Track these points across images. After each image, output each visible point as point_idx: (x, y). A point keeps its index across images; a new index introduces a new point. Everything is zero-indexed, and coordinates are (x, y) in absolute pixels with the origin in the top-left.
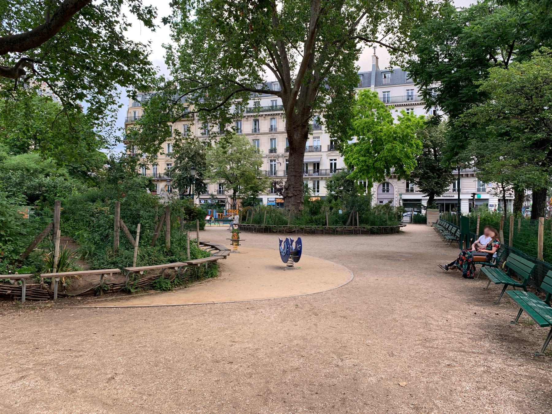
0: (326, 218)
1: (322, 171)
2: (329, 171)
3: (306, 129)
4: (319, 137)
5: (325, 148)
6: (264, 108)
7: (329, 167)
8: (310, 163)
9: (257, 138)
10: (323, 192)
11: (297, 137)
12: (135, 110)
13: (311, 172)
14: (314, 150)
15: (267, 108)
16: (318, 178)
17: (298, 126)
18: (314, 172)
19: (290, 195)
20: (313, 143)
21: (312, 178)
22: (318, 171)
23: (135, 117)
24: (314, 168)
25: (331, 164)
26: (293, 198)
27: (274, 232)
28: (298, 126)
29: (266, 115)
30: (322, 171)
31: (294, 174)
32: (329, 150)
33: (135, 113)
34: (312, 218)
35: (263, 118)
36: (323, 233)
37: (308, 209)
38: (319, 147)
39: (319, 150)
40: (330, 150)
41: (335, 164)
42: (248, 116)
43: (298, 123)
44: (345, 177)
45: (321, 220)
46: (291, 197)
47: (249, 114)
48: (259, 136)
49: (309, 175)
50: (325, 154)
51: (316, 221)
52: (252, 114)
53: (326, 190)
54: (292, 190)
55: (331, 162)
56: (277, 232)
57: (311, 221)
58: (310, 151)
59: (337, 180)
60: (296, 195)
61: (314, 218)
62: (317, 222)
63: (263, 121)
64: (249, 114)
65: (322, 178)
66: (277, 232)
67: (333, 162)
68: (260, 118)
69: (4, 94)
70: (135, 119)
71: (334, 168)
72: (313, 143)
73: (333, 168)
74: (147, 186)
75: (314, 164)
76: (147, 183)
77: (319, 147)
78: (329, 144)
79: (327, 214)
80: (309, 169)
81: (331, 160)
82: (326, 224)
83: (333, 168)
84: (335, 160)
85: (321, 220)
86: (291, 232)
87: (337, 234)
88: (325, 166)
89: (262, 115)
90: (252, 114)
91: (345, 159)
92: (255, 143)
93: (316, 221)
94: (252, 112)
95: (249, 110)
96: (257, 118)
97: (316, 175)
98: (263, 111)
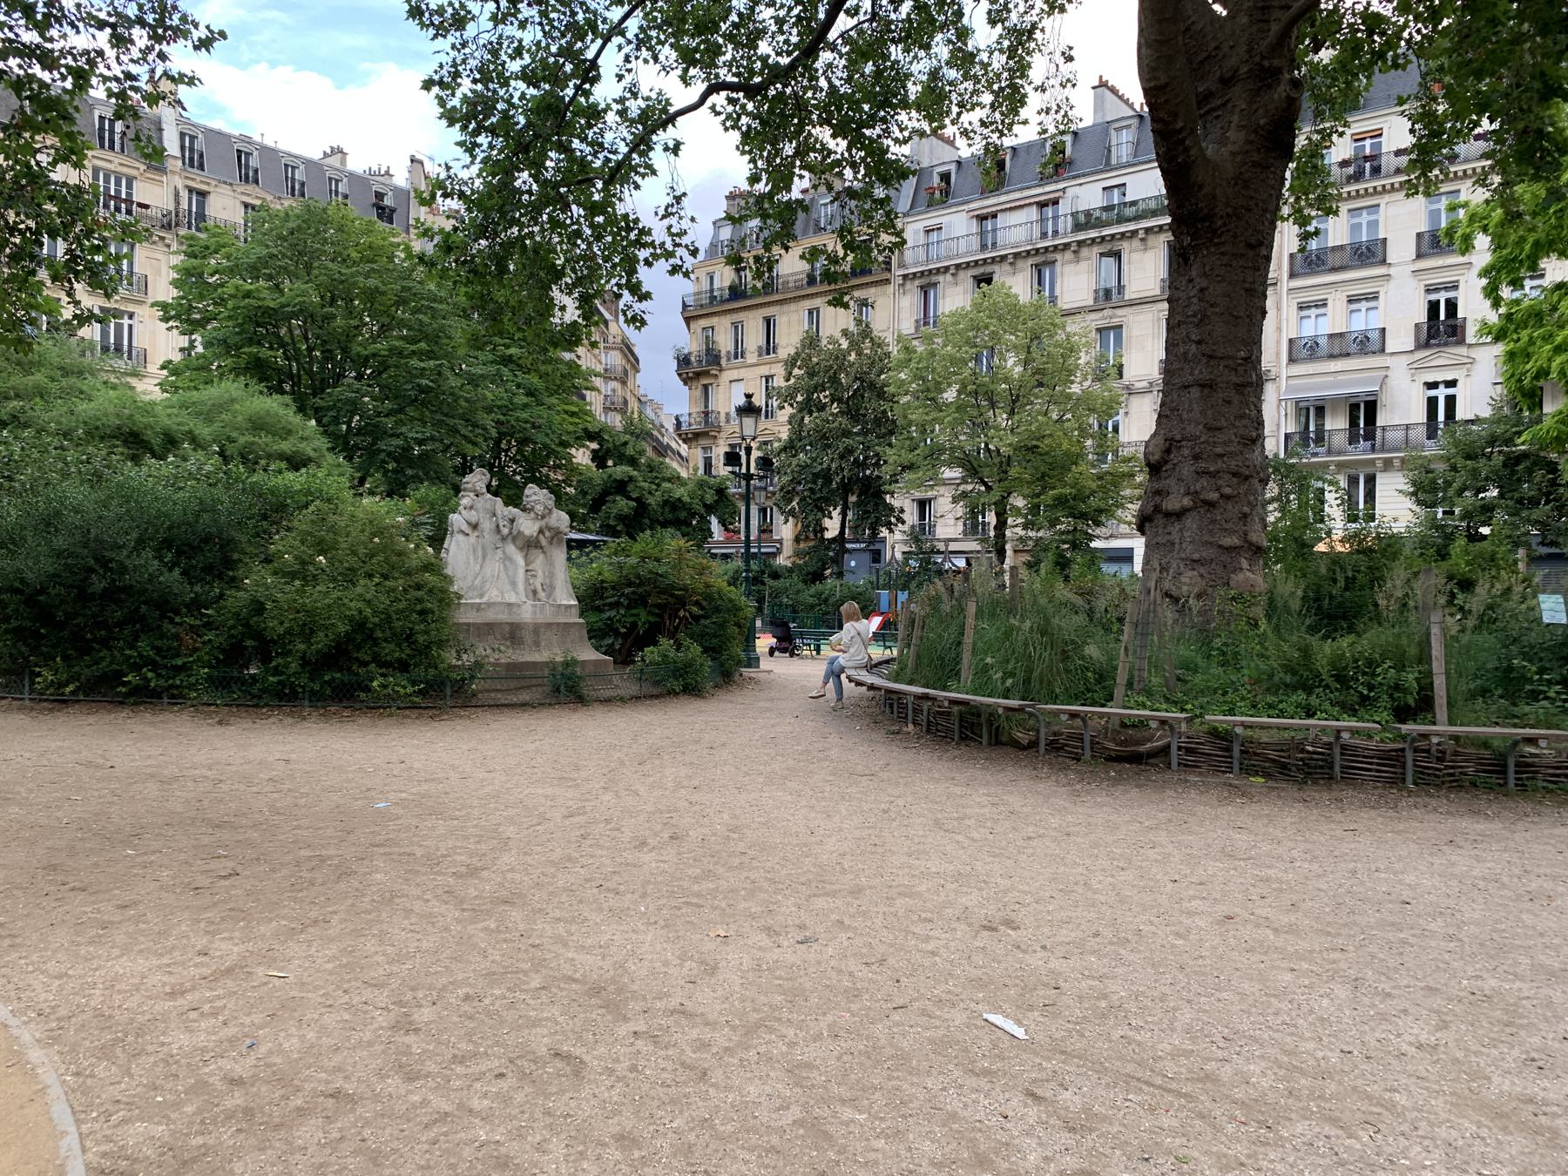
0: (1424, 657)
1: (1390, 435)
2: (1419, 434)
3: (1282, 90)
4: (1374, 297)
5: (1401, 338)
6: (1142, 206)
7: (1419, 415)
8: (1336, 401)
9: (1115, 322)
10: (1396, 508)
11: (1220, 145)
12: (710, 269)
13: (1340, 440)
14: (1354, 348)
15: (1153, 205)
16: (1373, 462)
17: (1226, 82)
18: (1353, 439)
19: (1172, 504)
20: (1349, 321)
21: (1341, 466)
22: (1370, 436)
23: (712, 291)
24: (1353, 422)
25: (1432, 402)
26: (1191, 522)
27: (1016, 744)
28: (1226, 82)
29: (1148, 230)
30: (1390, 435)
31: (1200, 372)
32: (1422, 345)
33: (712, 278)
34: (1306, 652)
35: (1136, 243)
36: (1397, 781)
37: (1291, 591)
38: (1375, 336)
39: (1377, 347)
40: (1427, 345)
41: (1451, 400)
42: (1080, 243)
43: (1233, 61)
44: (1509, 441)
45: (1387, 673)
46: (1179, 515)
47: (1081, 236)
48: (1119, 312)
49: (1329, 452)
50: (1405, 359)
51: (1341, 678)
52: (1093, 234)
53: (1409, 503)
54: (1187, 470)
55: (1433, 393)
56: (1033, 745)
57: (1301, 681)
58: (1332, 357)
59: (1468, 457)
60: (1210, 504)
61: (1325, 650)
62: (1349, 688)
63: (1136, 256)
64: (1081, 236)
65: (1388, 465)
66: (1033, 745)
67: (1441, 393)
68: (1125, 246)
69: (5, 128)
70: (713, 298)
71: (1441, 413)
72: (1349, 321)
73: (1441, 417)
74: (710, 509)
75: (1354, 408)
76: (710, 497)
77: (1375, 336)
78: (1422, 317)
79: (1440, 628)
80: (1327, 427)
81: (1432, 385)
82: (1425, 705)
83: (1441, 417)
84: (1452, 384)
85: (1387, 673)
86: (1136, 759)
87: (1522, 787)
88: (1404, 408)
89: (1134, 233)
90: (1093, 234)
91: (1511, 356)
92: (1104, 344)
93: (1341, 678)
94: (1094, 227)
95: (1082, 218)
96: (1116, 246)
97: (1361, 452)
98: (1137, 218)
